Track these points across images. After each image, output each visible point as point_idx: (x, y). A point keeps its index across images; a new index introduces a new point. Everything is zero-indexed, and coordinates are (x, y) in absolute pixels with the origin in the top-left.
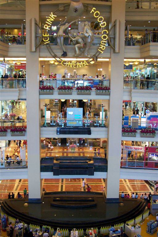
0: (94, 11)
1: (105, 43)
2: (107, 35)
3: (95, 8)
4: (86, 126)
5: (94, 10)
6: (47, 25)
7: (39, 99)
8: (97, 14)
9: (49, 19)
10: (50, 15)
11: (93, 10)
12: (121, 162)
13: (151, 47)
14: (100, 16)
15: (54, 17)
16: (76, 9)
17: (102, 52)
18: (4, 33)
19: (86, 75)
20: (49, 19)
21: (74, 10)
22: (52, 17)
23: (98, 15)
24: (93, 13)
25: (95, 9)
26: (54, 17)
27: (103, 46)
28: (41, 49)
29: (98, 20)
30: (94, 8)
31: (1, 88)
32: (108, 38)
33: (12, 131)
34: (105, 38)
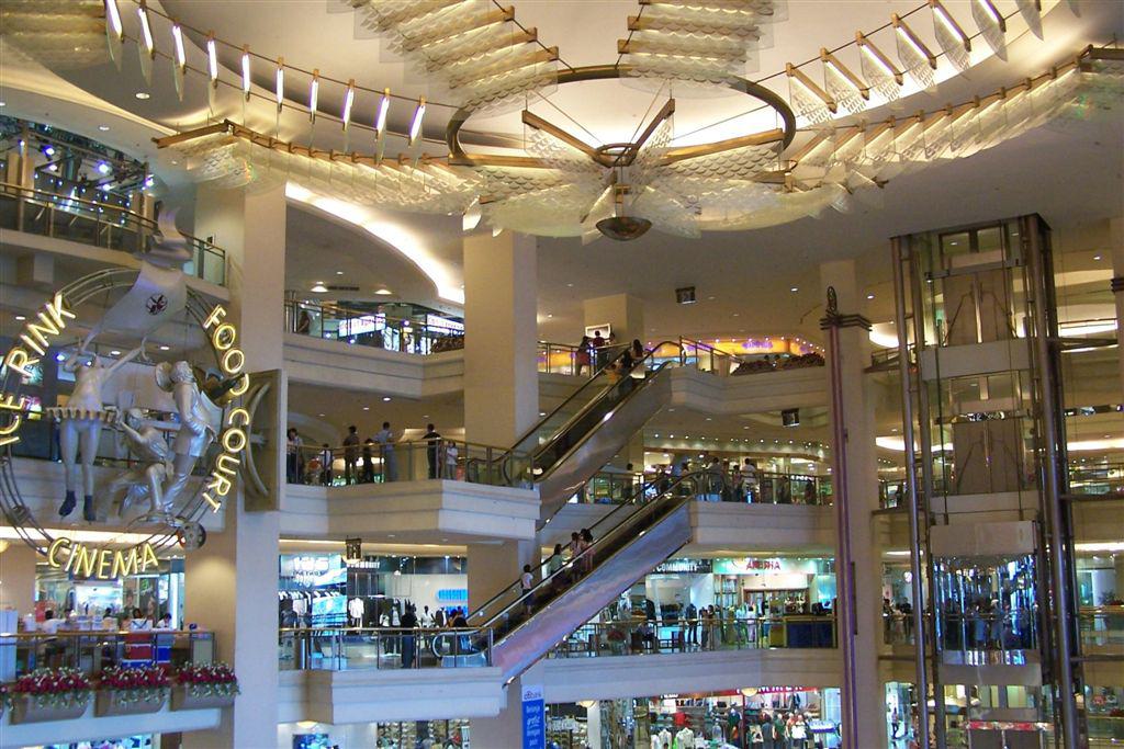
3: (225, 309)
6: (24, 354)
8: (226, 337)
10: (49, 306)
11: (214, 319)
13: (444, 495)
15: (62, 316)
16: (160, 299)
17: (217, 506)
18: (28, 427)
19: (353, 429)
21: (151, 304)
23: (229, 340)
24: (214, 326)
25: (224, 313)
27: (222, 479)
28: (696, 513)
32: (244, 448)
33: (607, 208)
34: (230, 440)
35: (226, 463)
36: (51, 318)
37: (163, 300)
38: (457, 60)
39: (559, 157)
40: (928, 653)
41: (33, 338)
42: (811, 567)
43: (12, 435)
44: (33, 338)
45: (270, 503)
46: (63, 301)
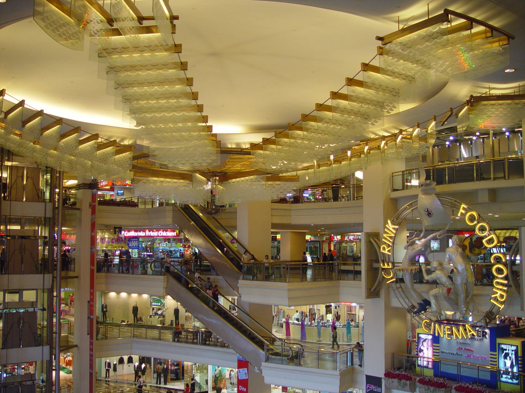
0: (463, 212)
1: (502, 284)
2: (505, 264)
4: (408, 365)
5: (464, 208)
7: (91, 252)
8: (472, 219)
9: (387, 233)
11: (462, 211)
12: (79, 127)
14: (478, 223)
15: (394, 229)
20: (387, 233)
22: (391, 229)
24: (463, 215)
26: (394, 229)
27: (500, 292)
29: (484, 224)
30: (463, 206)
31: (359, 342)
35: (498, 283)
36: (389, 229)
37: (429, 210)
38: (146, 112)
39: (409, 74)
40: (54, 350)
41: (386, 239)
42: (435, 308)
43: (392, 278)
44: (386, 239)
45: (377, 295)
46: (391, 223)
